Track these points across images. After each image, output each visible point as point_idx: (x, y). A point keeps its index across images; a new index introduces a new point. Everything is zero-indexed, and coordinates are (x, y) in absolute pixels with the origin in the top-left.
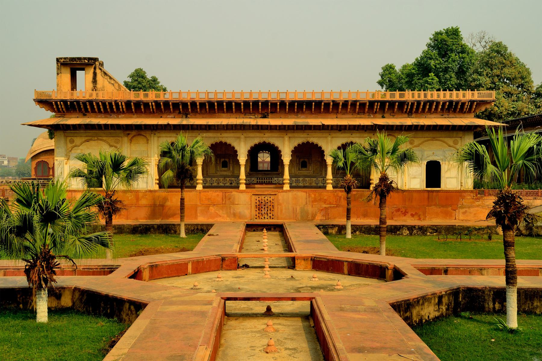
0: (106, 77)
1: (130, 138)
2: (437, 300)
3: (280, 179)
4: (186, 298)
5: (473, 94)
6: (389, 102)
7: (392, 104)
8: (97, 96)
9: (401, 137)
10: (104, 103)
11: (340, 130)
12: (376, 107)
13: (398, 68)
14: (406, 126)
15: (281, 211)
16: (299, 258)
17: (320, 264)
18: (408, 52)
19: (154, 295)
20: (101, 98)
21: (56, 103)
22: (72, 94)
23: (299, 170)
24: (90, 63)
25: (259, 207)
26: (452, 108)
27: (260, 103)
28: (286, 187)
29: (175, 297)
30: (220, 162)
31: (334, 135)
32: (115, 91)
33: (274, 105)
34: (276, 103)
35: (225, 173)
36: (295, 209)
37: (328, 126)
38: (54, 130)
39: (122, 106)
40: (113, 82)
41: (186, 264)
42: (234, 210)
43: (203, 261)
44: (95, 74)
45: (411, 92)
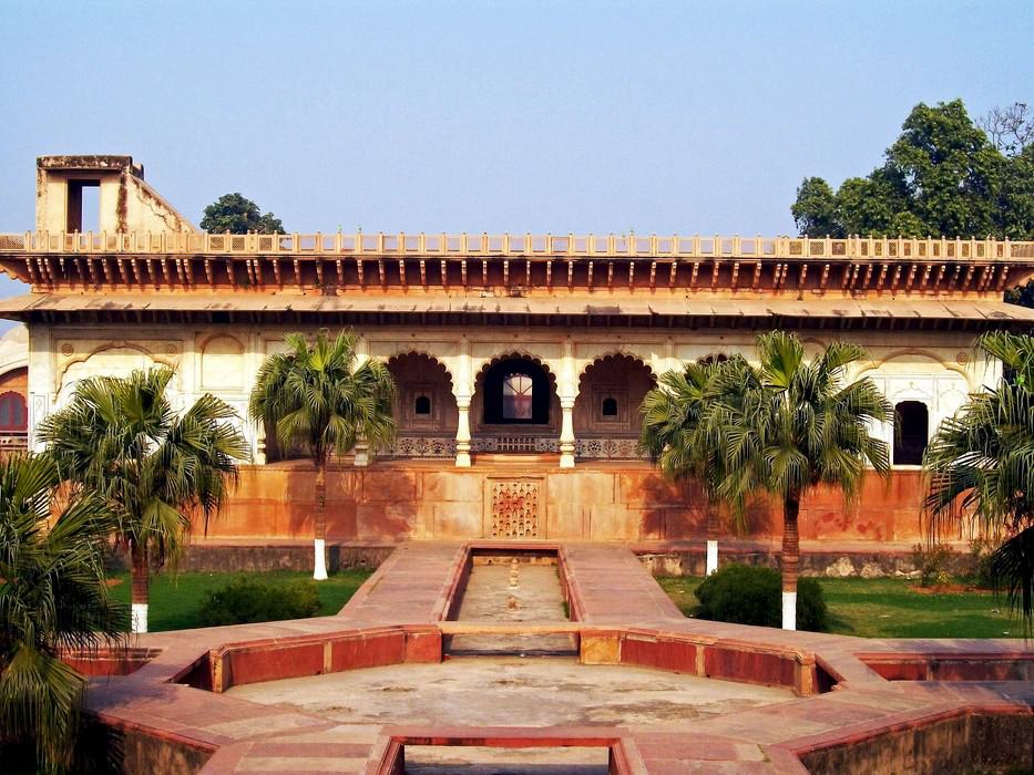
0: (149, 201)
1: (201, 342)
2: (911, 742)
3: (552, 441)
4: (308, 739)
5: (1000, 249)
6: (831, 262)
7: (816, 268)
8: (126, 245)
9: (842, 344)
10: (142, 263)
11: (694, 328)
12: (778, 275)
13: (835, 186)
14: (848, 319)
15: (555, 516)
16: (591, 634)
17: (637, 652)
18: (858, 152)
19: (230, 729)
20: (132, 249)
21: (34, 261)
22: (69, 241)
23: (599, 420)
24: (115, 169)
25: (507, 506)
26: (955, 277)
27: (506, 263)
28: (567, 461)
29: (281, 734)
30: (411, 401)
31: (679, 339)
32: (169, 232)
33: (539, 266)
34: (545, 264)
35: (424, 426)
36: (587, 514)
37: (666, 317)
38: (35, 320)
39: (183, 267)
40: (163, 211)
41: (319, 649)
42: (442, 513)
43: (359, 641)
44: (123, 194)
45: (859, 241)
